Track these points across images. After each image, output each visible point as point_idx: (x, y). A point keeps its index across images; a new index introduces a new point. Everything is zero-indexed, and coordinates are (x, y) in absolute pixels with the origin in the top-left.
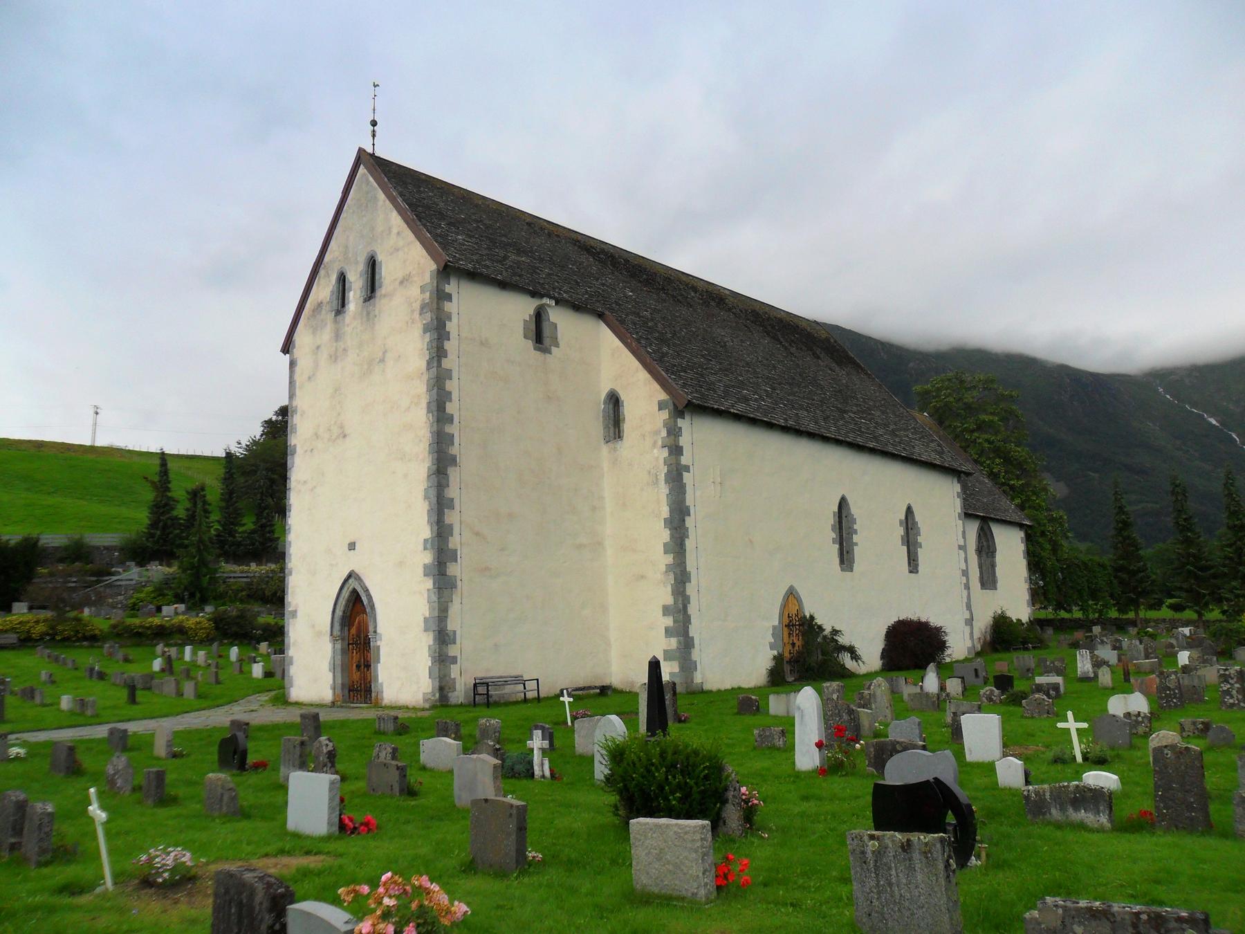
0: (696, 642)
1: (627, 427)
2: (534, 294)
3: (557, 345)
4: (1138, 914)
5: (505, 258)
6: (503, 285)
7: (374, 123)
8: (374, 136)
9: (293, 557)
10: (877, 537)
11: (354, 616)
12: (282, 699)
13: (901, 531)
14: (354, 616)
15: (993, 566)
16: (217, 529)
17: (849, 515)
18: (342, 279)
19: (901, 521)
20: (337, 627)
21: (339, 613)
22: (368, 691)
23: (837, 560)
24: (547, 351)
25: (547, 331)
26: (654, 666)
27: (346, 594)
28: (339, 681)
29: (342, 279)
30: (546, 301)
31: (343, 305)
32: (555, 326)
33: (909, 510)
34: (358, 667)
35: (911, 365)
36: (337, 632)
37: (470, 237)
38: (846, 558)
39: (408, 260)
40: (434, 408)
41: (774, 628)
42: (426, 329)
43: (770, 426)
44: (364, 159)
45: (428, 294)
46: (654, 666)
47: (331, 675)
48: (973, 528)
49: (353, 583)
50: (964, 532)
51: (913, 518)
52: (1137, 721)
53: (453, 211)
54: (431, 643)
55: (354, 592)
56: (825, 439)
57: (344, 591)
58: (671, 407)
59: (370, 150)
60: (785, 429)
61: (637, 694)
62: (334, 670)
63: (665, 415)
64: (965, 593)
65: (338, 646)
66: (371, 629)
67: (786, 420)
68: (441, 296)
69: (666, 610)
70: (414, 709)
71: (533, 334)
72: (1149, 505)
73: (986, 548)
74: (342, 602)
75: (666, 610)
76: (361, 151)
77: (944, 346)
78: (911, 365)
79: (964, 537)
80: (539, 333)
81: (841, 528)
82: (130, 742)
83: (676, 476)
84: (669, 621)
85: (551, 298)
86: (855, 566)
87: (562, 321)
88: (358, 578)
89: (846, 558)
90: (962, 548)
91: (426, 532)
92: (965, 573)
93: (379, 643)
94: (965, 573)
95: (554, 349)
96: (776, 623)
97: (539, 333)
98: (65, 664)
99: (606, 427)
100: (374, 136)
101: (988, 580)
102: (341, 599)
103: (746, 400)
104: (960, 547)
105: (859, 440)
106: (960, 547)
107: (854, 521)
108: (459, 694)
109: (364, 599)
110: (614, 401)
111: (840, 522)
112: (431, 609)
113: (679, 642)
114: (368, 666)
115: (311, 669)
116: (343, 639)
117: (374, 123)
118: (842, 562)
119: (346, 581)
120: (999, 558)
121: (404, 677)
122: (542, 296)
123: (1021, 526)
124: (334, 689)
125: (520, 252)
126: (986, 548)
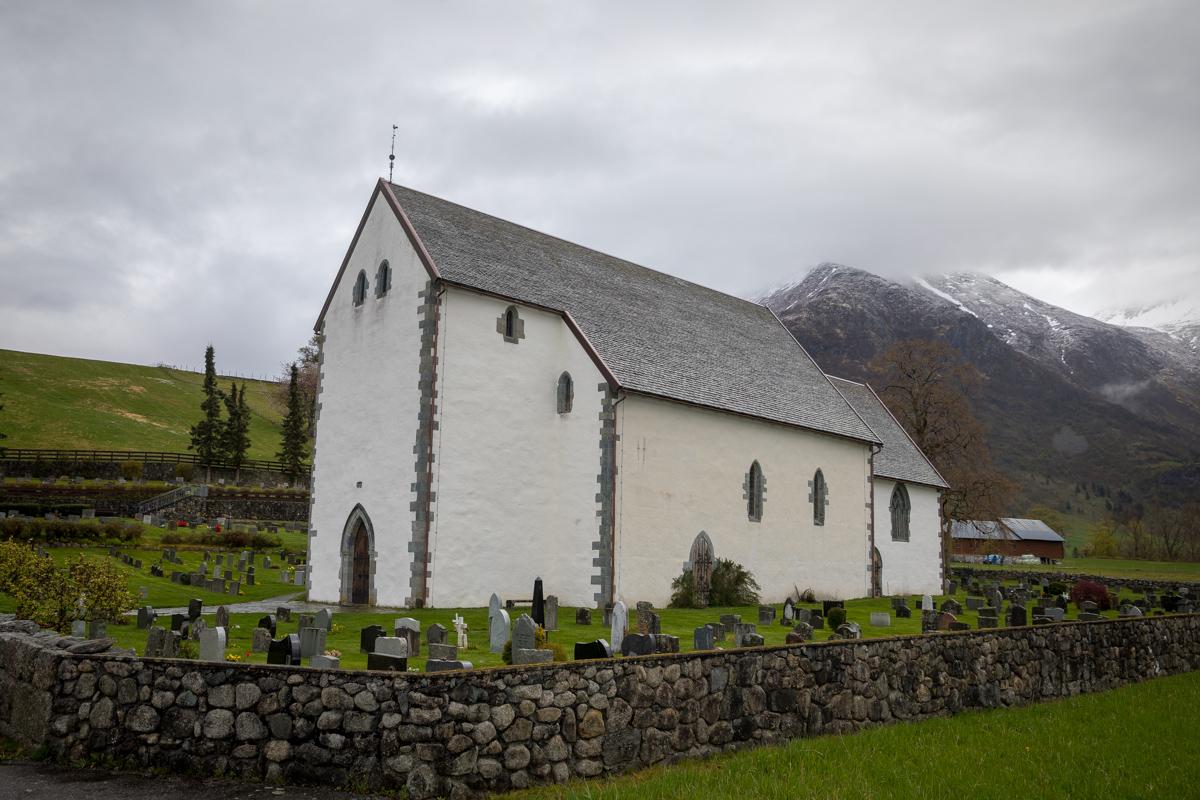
3: (523, 337)
7: (392, 157)
8: (392, 167)
9: (337, 573)
10: (786, 492)
11: (359, 537)
12: (304, 599)
13: (810, 490)
14: (359, 537)
15: (907, 521)
16: (240, 449)
18: (362, 277)
19: (810, 484)
20: (346, 545)
21: (348, 534)
23: (746, 512)
24: (516, 342)
25: (516, 326)
26: (538, 584)
27: (354, 520)
29: (362, 277)
31: (362, 299)
32: (523, 322)
36: (346, 549)
38: (755, 510)
44: (381, 186)
46: (538, 584)
51: (823, 480)
55: (360, 519)
57: (353, 517)
58: (608, 389)
59: (388, 179)
62: (342, 576)
63: (602, 395)
65: (346, 560)
70: (396, 608)
71: (504, 329)
72: (1171, 463)
74: (351, 526)
75: (595, 546)
81: (752, 486)
83: (609, 442)
84: (596, 554)
86: (763, 517)
88: (362, 509)
89: (755, 510)
92: (871, 527)
95: (520, 340)
96: (687, 560)
98: (138, 565)
99: (559, 401)
100: (392, 167)
102: (350, 524)
107: (765, 481)
110: (566, 381)
111: (752, 482)
113: (602, 571)
114: (367, 577)
115: (326, 582)
116: (350, 555)
117: (392, 157)
118: (751, 512)
120: (912, 515)
121: (391, 589)
124: (341, 591)
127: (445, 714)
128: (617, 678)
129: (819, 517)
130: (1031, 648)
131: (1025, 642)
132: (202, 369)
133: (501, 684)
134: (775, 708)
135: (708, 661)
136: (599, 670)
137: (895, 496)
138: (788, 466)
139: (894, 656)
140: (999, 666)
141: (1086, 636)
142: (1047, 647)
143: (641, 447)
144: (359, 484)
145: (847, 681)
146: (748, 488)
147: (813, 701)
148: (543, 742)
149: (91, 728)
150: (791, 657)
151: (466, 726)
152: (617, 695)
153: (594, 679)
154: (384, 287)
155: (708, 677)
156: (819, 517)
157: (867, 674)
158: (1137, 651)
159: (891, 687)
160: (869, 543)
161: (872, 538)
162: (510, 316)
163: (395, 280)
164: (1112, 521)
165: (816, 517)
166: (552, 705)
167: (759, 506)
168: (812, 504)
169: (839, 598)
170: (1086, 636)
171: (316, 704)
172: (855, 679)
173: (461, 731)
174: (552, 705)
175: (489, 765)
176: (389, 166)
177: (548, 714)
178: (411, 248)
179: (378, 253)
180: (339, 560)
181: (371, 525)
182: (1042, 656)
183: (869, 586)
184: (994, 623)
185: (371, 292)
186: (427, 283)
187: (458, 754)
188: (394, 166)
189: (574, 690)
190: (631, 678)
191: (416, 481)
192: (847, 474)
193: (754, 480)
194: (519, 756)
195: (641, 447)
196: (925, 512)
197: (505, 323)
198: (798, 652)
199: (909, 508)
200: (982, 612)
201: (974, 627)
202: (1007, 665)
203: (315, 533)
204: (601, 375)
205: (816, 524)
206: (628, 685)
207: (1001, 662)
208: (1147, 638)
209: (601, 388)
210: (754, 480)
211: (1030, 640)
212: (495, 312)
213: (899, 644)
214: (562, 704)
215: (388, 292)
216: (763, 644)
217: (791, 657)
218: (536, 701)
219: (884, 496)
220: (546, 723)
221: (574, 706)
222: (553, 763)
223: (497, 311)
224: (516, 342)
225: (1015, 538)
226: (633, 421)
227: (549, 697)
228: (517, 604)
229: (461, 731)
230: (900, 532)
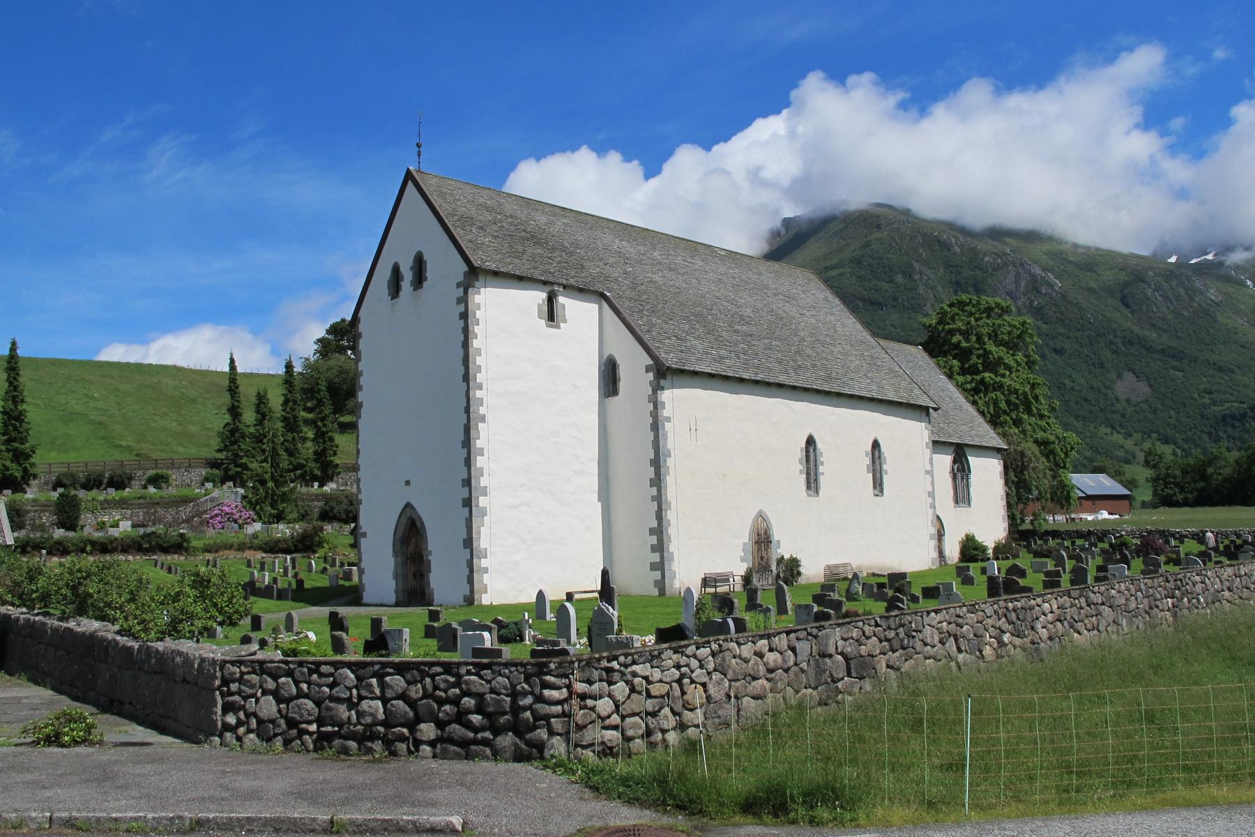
0: (675, 556)
1: (622, 386)
2: (545, 283)
4: (933, 768)
7: (419, 146)
13: (868, 461)
18: (396, 271)
19: (867, 454)
20: (398, 545)
21: (399, 534)
22: (423, 593)
23: (804, 488)
24: (558, 327)
27: (404, 520)
28: (401, 586)
29: (396, 271)
34: (415, 576)
35: (987, 259)
38: (812, 483)
41: (745, 544)
50: (931, 459)
63: (651, 376)
65: (399, 560)
69: (822, 463)
73: (961, 470)
78: (987, 259)
80: (551, 315)
81: (808, 461)
85: (559, 284)
88: (413, 508)
90: (930, 473)
92: (931, 494)
94: (931, 494)
97: (551, 315)
101: (962, 496)
104: (927, 472)
106: (927, 472)
109: (418, 524)
111: (807, 456)
114: (422, 575)
118: (808, 488)
120: (973, 478)
122: (552, 284)
124: (396, 592)
126: (961, 470)
127: (571, 693)
128: (713, 654)
129: (878, 485)
130: (1088, 605)
131: (1083, 600)
132: (227, 369)
133: (615, 664)
134: (854, 674)
135: (793, 635)
136: (698, 648)
137: (955, 461)
138: (845, 431)
139: (960, 621)
140: (1058, 624)
141: (1140, 590)
142: (1103, 604)
143: (693, 428)
144: (408, 483)
145: (919, 645)
147: (888, 666)
148: (654, 714)
150: (866, 628)
151: (590, 702)
152: (715, 670)
153: (695, 656)
155: (793, 649)
156: (878, 485)
157: (936, 639)
158: (1189, 601)
159: (959, 650)
160: (931, 512)
161: (933, 506)
162: (551, 299)
163: (430, 272)
165: (875, 488)
166: (661, 681)
168: (871, 475)
169: (903, 570)
170: (1140, 590)
172: (926, 645)
173: (585, 707)
174: (661, 681)
175: (612, 736)
177: (656, 689)
178: (446, 237)
180: (392, 560)
182: (1098, 614)
183: (935, 555)
184: (1058, 584)
185: (406, 284)
187: (585, 727)
189: (678, 667)
190: (727, 653)
192: (907, 438)
194: (635, 725)
195: (693, 428)
196: (988, 474)
198: (873, 622)
200: (1047, 574)
201: (1038, 588)
202: (1066, 623)
206: (724, 660)
207: (1060, 621)
208: (1199, 587)
209: (648, 369)
211: (1087, 599)
212: (538, 297)
213: (965, 609)
214: (668, 680)
215: (425, 284)
216: (500, 656)
217: (866, 628)
218: (646, 678)
219: (945, 461)
220: (656, 697)
221: (679, 681)
222: (664, 731)
223: (540, 296)
224: (558, 327)
225: (1081, 495)
226: (676, 399)
227: (657, 674)
228: (577, 596)
229: (585, 707)
230: (962, 496)
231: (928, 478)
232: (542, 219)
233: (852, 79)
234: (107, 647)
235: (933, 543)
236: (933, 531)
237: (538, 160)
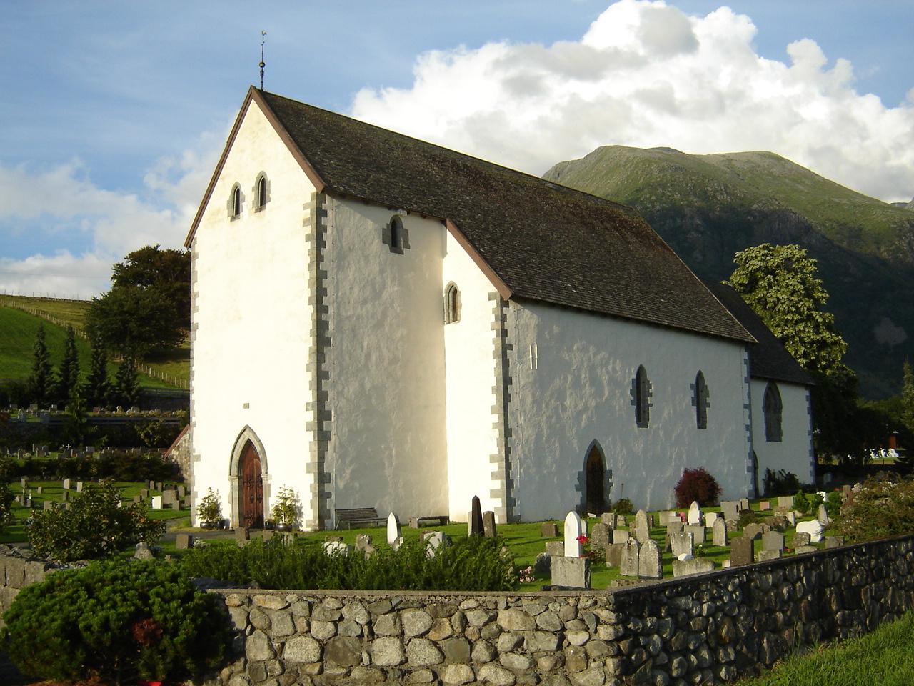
1: (463, 312)
5: (368, 176)
6: (366, 202)
8: (262, 75)
10: (671, 404)
11: (249, 465)
13: (692, 393)
14: (249, 465)
15: (779, 420)
17: (646, 382)
18: (237, 192)
19: (692, 386)
21: (236, 458)
26: (476, 502)
27: (242, 443)
29: (237, 192)
30: (400, 212)
33: (700, 377)
37: (341, 160)
38: (642, 417)
39: (295, 186)
40: (314, 301)
42: (308, 238)
43: (579, 311)
45: (309, 211)
46: (476, 502)
47: (230, 505)
48: (760, 389)
49: (247, 435)
50: (749, 394)
52: (801, 538)
53: (325, 137)
54: (313, 482)
56: (627, 320)
58: (499, 299)
60: (593, 313)
61: (467, 523)
64: (748, 445)
66: (263, 471)
67: (593, 305)
68: (320, 213)
71: (389, 239)
73: (773, 407)
76: (253, 87)
77: (441, 432)
79: (749, 397)
82: (322, 484)
85: (403, 209)
87: (410, 223)
89: (642, 417)
90: (748, 407)
91: (309, 396)
93: (269, 482)
94: (749, 428)
100: (262, 75)
101: (774, 433)
102: (237, 447)
103: (559, 289)
104: (745, 406)
105: (656, 319)
106: (745, 406)
108: (282, 570)
112: (312, 456)
117: (263, 65)
118: (639, 420)
119: (242, 433)
120: (784, 414)
122: (396, 209)
123: (807, 386)
125: (379, 169)
126: (773, 407)
129: (702, 422)
144: (247, 406)
146: (635, 394)
149: (142, 643)
154: (262, 200)
156: (702, 422)
163: (273, 192)
164: (650, 541)
167: (646, 412)
171: (493, 627)
176: (259, 74)
179: (754, 469)
181: (262, 447)
183: (751, 487)
186: (312, 194)
188: (265, 74)
191: (495, 385)
193: (640, 388)
197: (390, 234)
199: (781, 408)
203: (198, 458)
204: (296, 162)
205: (699, 427)
210: (640, 388)
215: (268, 205)
231: (747, 411)
232: (344, 124)
233: (415, 73)
234: (162, 256)
235: (749, 476)
236: (747, 462)
237: (596, 20)
